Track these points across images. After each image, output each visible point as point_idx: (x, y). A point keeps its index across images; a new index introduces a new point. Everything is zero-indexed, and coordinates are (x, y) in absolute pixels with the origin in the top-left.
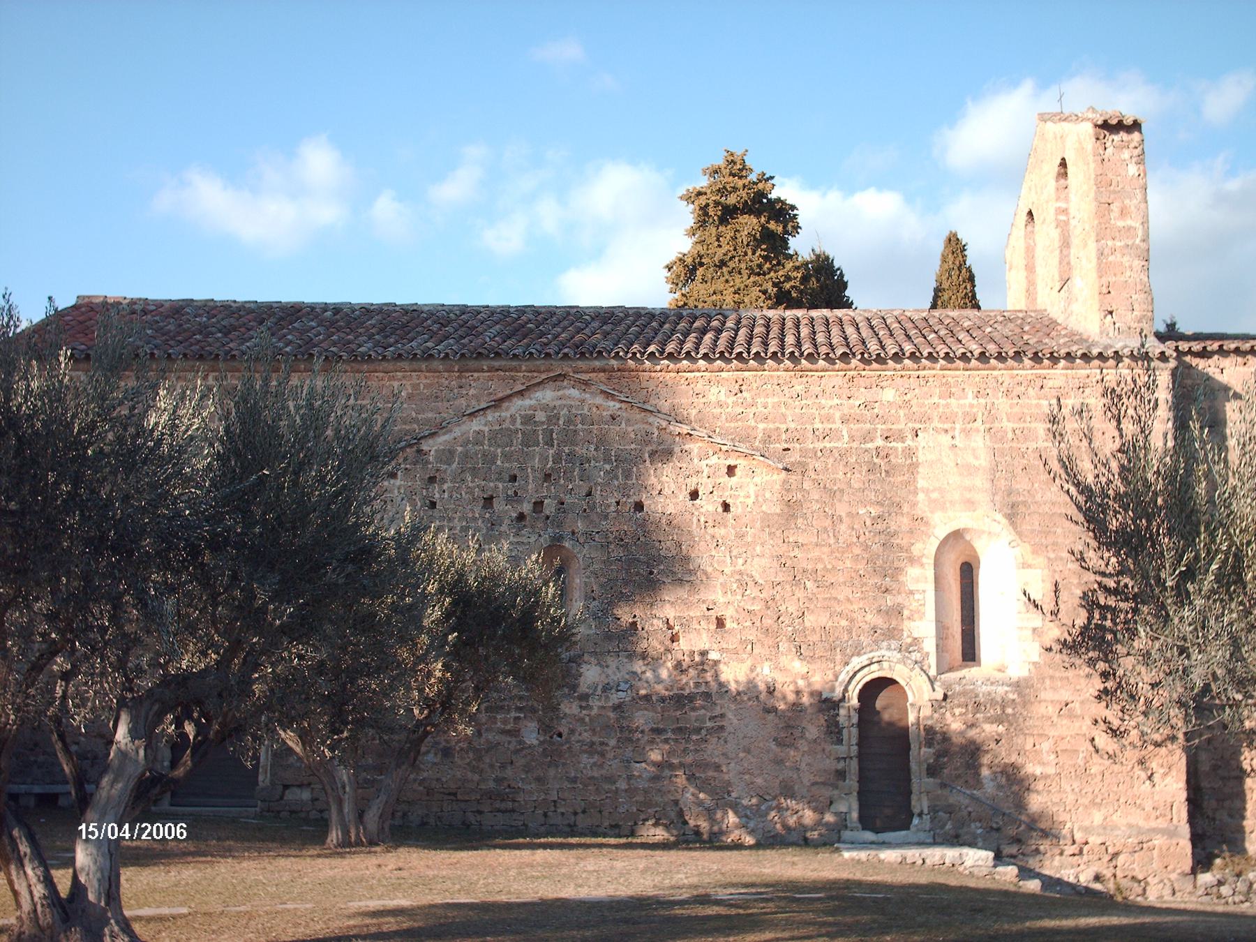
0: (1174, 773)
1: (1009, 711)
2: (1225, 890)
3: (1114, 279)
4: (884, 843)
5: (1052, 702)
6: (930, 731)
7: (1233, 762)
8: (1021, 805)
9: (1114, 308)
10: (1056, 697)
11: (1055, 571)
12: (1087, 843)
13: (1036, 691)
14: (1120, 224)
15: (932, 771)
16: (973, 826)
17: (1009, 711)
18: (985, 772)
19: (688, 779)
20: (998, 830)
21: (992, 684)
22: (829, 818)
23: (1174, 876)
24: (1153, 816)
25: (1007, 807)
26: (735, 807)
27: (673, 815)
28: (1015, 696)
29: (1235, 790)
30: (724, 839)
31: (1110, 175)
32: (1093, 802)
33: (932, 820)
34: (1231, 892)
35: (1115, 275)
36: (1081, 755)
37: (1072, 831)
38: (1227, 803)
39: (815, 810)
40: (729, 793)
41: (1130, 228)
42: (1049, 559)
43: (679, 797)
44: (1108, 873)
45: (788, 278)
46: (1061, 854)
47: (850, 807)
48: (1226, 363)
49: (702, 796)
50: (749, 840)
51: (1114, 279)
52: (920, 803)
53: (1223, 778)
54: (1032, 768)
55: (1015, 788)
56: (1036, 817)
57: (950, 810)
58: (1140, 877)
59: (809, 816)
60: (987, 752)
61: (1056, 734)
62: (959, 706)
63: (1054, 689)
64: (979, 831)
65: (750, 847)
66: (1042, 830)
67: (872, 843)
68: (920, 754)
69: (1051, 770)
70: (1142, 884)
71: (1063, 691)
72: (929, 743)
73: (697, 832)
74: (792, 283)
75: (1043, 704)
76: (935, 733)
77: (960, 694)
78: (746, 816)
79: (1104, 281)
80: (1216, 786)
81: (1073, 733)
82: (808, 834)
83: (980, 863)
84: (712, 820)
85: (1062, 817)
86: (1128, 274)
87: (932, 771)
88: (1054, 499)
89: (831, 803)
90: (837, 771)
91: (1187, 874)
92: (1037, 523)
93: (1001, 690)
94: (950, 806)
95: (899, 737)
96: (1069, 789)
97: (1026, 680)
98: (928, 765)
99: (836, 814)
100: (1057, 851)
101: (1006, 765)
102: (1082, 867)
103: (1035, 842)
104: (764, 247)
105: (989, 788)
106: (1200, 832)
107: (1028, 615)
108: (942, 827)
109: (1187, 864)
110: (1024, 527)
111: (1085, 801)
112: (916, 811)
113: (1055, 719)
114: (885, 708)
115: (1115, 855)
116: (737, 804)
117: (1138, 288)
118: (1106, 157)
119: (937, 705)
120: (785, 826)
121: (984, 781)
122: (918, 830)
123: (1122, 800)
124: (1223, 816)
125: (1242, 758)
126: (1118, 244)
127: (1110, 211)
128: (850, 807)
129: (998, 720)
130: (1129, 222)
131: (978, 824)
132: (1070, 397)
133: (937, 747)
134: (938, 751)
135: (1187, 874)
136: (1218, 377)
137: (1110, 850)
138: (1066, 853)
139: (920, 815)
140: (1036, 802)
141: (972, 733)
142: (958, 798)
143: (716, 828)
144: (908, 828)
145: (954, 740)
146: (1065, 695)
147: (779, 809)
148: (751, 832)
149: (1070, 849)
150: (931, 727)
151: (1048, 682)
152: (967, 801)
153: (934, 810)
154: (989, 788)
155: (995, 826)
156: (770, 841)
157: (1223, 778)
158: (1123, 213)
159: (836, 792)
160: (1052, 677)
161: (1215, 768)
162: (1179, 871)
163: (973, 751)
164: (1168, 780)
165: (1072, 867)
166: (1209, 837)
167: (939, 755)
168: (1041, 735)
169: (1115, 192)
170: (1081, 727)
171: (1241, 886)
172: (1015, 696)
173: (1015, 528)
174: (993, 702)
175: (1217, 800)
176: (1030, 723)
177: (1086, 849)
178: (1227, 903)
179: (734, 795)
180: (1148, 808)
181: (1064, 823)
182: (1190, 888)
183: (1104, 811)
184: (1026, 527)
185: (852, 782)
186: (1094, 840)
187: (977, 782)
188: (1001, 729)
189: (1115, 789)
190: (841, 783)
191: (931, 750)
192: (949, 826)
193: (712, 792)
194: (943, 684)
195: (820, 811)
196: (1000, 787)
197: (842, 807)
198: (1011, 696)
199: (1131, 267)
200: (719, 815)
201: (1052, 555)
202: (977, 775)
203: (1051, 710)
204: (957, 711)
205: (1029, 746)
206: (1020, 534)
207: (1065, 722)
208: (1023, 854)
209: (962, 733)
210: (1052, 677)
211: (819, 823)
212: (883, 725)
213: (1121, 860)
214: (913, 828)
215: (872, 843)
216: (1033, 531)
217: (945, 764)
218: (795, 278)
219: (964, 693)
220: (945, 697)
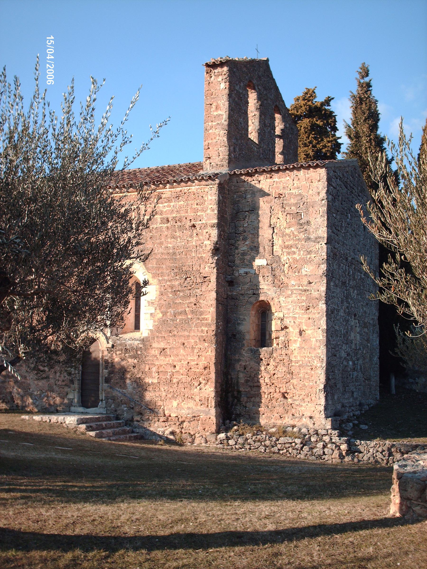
0: (209, 383)
1: (139, 353)
2: (231, 442)
3: (211, 141)
4: (87, 413)
5: (157, 348)
6: (106, 362)
7: (256, 379)
8: (142, 397)
9: (211, 155)
10: (159, 346)
11: (161, 286)
12: (170, 416)
13: (150, 343)
14: (215, 113)
15: (107, 380)
16: (123, 406)
17: (139, 353)
18: (128, 381)
19: (15, 383)
20: (133, 408)
21: (133, 340)
22: (66, 401)
23: (208, 434)
24: (199, 404)
25: (136, 398)
26: (31, 395)
27: (9, 398)
28: (142, 346)
29: (256, 393)
30: (26, 409)
31: (212, 90)
32: (173, 396)
33: (106, 403)
34: (234, 443)
35: (212, 139)
36: (169, 374)
37: (164, 410)
38: (253, 399)
39: (61, 397)
40: (30, 389)
41: (219, 115)
42: (159, 280)
43: (11, 390)
44: (178, 431)
45: (325, 146)
46: (158, 421)
47: (74, 397)
48: (261, 178)
49: (20, 390)
50: (36, 410)
51: (211, 141)
52: (102, 396)
53: (251, 387)
54: (148, 380)
55: (140, 389)
56: (149, 403)
57: (114, 399)
58: (192, 433)
59: (58, 400)
60: (129, 372)
61: (159, 364)
62: (119, 350)
63: (158, 342)
64: (125, 409)
65: (36, 412)
66: (150, 409)
67: (82, 413)
68: (104, 372)
69: (155, 381)
70: (193, 437)
71: (162, 344)
72: (106, 368)
73: (17, 406)
74: (327, 149)
75: (154, 349)
76: (109, 363)
77: (119, 345)
78: (36, 399)
79: (206, 143)
80: (247, 390)
81: (165, 363)
82: (58, 408)
83: (72, 422)
84: (22, 401)
85: (160, 403)
86: (218, 138)
87: (107, 380)
88: (163, 251)
89: (67, 394)
90: (70, 380)
91: (214, 433)
92: (155, 263)
93: (136, 343)
94: (114, 397)
95: (96, 364)
96: (163, 390)
97: (147, 338)
98: (106, 378)
99: (69, 399)
100: (156, 419)
101: (137, 378)
102: (167, 427)
103: (147, 414)
104: (313, 133)
105: (130, 388)
106: (238, 413)
107: (149, 307)
108: (110, 407)
109: (214, 428)
110: (149, 265)
111: (170, 396)
112: (100, 398)
113: (158, 356)
114: (93, 352)
115: (183, 422)
116: (32, 394)
117: (222, 144)
118: (210, 81)
119: (109, 350)
120: (50, 405)
121: (128, 385)
122: (100, 408)
123: (186, 396)
124: (250, 405)
125: (260, 376)
126: (214, 124)
127: (211, 108)
128: (74, 397)
129: (135, 357)
130: (220, 112)
131: (125, 405)
132: (172, 202)
133: (109, 369)
134: (110, 371)
135: (214, 433)
136: (257, 186)
137: (180, 420)
138: (161, 420)
139: (102, 400)
140: (149, 396)
141: (123, 363)
142: (117, 392)
143: (24, 404)
144: (97, 407)
145: (116, 366)
146: (162, 345)
147: (48, 397)
148: (37, 407)
149: (162, 419)
150: (107, 360)
151: (156, 339)
152: (120, 395)
153: (107, 398)
154: (130, 388)
155: (131, 406)
156: (45, 411)
157: (251, 387)
158: (217, 108)
159: (69, 389)
160: (157, 337)
161: (247, 381)
162: (210, 431)
163: (123, 371)
164: (207, 387)
165: (163, 427)
166: (242, 416)
167: (110, 373)
168: (152, 364)
169: (214, 98)
170: (169, 360)
171: (241, 440)
172: (142, 346)
173: (145, 266)
174: (133, 348)
175: (248, 397)
176: (147, 358)
177: (170, 418)
178: (232, 448)
179: (31, 390)
180: (197, 400)
181: (160, 406)
182: (214, 440)
183: (177, 401)
184: (150, 266)
185: (76, 385)
186: (173, 415)
187: (124, 386)
188: (136, 361)
189: (183, 390)
190: (72, 385)
191: (107, 371)
192: (113, 406)
193: (23, 389)
194: (113, 340)
195: (63, 398)
196: (134, 388)
197: (70, 396)
198: (140, 346)
199: (219, 135)
200: (25, 398)
201: (160, 278)
202: (125, 382)
203: (157, 353)
204: (118, 353)
205: (147, 369)
206: (147, 269)
207: (162, 358)
208: (143, 420)
209: (119, 363)
210: (157, 337)
211: (62, 403)
212: (92, 359)
213: (185, 424)
214: (99, 407)
215: (82, 413)
216: (153, 267)
217: (112, 377)
218: (329, 146)
219: (121, 345)
220: (113, 346)
